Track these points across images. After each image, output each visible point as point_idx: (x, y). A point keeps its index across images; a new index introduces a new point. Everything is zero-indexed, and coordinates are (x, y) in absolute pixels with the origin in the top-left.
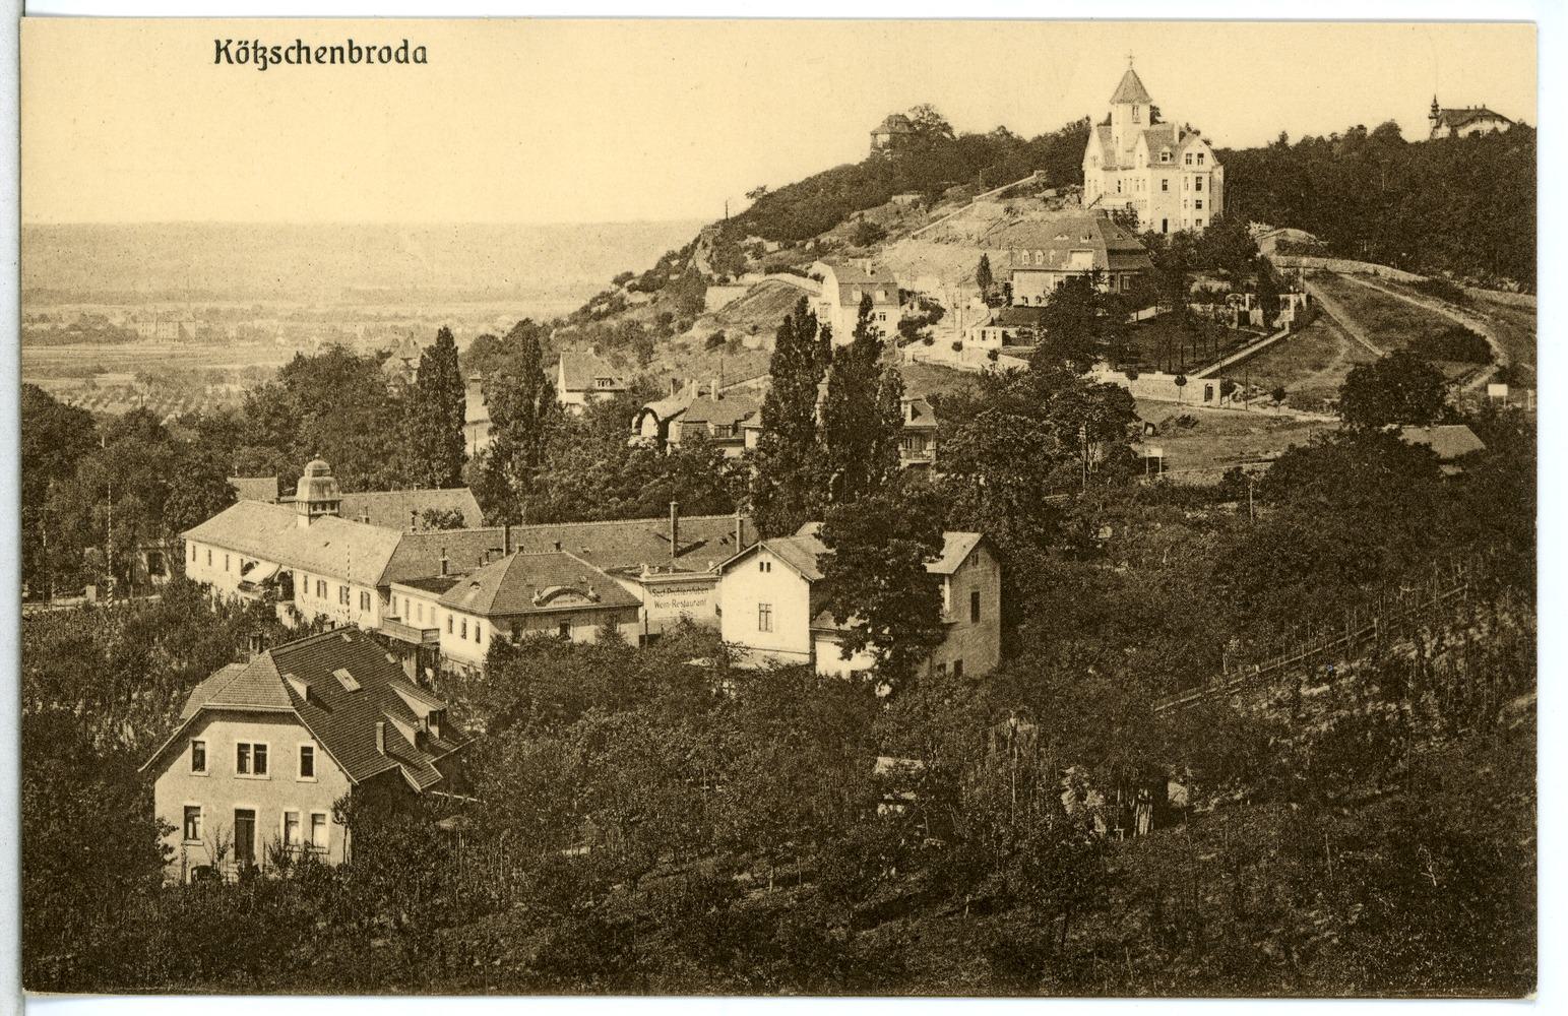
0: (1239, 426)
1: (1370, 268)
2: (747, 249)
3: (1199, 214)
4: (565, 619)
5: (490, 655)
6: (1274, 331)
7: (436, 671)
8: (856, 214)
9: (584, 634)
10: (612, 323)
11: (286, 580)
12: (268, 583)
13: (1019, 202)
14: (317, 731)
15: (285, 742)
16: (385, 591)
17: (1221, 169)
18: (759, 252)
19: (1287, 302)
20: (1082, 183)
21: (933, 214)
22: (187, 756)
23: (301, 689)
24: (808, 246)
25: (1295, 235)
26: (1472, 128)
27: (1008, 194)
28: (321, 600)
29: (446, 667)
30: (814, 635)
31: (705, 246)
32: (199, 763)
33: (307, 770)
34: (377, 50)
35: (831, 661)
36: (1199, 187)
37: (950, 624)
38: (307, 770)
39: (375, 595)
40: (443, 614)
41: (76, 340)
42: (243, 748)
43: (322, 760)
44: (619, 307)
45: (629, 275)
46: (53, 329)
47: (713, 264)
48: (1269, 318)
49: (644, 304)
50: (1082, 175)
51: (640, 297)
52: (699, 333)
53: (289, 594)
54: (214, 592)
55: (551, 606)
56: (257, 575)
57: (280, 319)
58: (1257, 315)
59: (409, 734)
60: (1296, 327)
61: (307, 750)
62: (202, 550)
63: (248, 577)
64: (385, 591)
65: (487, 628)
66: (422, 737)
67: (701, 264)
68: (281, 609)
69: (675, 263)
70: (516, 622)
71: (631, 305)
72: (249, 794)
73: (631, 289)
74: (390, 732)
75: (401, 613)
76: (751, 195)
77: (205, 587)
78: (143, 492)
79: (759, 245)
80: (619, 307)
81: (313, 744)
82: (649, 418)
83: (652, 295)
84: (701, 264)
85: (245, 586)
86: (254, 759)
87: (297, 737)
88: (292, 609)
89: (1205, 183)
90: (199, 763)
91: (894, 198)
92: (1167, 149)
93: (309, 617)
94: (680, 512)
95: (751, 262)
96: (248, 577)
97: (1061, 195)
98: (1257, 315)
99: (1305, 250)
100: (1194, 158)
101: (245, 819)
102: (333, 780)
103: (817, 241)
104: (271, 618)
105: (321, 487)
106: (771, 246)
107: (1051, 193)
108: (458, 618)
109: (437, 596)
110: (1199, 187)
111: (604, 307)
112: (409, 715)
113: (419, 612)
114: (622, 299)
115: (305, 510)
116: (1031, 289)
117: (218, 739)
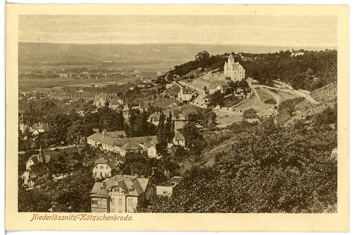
0: (234, 116)
2: (174, 77)
4: (134, 150)
5: (126, 154)
6: (246, 99)
7: (120, 156)
8: (192, 71)
10: (151, 89)
11: (101, 144)
12: (99, 145)
13: (214, 74)
14: (108, 165)
15: (105, 166)
16: (113, 146)
17: (245, 70)
18: (176, 77)
19: (248, 94)
20: (224, 71)
21: (202, 74)
22: (96, 167)
23: (106, 161)
24: (184, 76)
25: (255, 81)
26: (297, 54)
28: (105, 147)
29: (120, 156)
30: (156, 154)
31: (167, 76)
32: (97, 168)
33: (107, 168)
34: (120, 218)
36: (240, 73)
37: (170, 153)
38: (107, 168)
39: (112, 147)
41: (46, 77)
42: (101, 167)
43: (109, 167)
44: (152, 86)
46: (41, 75)
47: (168, 79)
48: (246, 97)
49: (156, 86)
50: (224, 70)
51: (156, 84)
52: (164, 94)
53: (101, 146)
54: (91, 145)
55: (133, 149)
56: (97, 144)
57: (89, 71)
58: (244, 96)
59: (117, 165)
60: (249, 98)
61: (107, 167)
62: (90, 140)
63: (96, 144)
64: (113, 146)
65: (125, 151)
66: (118, 165)
67: (166, 79)
68: (100, 148)
69: (162, 78)
70: (129, 150)
71: (154, 86)
72: (102, 170)
73: (154, 83)
74: (115, 165)
75: (115, 149)
76: (174, 67)
77: (91, 145)
78: (81, 132)
79: (176, 76)
80: (152, 86)
81: (107, 166)
82: (150, 117)
83: (158, 84)
84: (166, 79)
85: (96, 145)
86: (102, 167)
87: (106, 165)
88: (102, 148)
90: (97, 168)
91: (198, 68)
92: (236, 67)
93: (104, 149)
94: (149, 136)
95: (174, 79)
96: (96, 144)
97: (221, 73)
98: (244, 96)
99: (256, 84)
100: (240, 69)
101: (101, 173)
102: (110, 170)
103: (185, 76)
104: (99, 149)
105: (105, 133)
106: (178, 76)
107: (219, 73)
108: (122, 150)
109: (120, 147)
110: (240, 73)
111: (150, 86)
112: (117, 163)
113: (117, 149)
114: (153, 84)
115: (103, 135)
116: (212, 92)
117: (99, 166)
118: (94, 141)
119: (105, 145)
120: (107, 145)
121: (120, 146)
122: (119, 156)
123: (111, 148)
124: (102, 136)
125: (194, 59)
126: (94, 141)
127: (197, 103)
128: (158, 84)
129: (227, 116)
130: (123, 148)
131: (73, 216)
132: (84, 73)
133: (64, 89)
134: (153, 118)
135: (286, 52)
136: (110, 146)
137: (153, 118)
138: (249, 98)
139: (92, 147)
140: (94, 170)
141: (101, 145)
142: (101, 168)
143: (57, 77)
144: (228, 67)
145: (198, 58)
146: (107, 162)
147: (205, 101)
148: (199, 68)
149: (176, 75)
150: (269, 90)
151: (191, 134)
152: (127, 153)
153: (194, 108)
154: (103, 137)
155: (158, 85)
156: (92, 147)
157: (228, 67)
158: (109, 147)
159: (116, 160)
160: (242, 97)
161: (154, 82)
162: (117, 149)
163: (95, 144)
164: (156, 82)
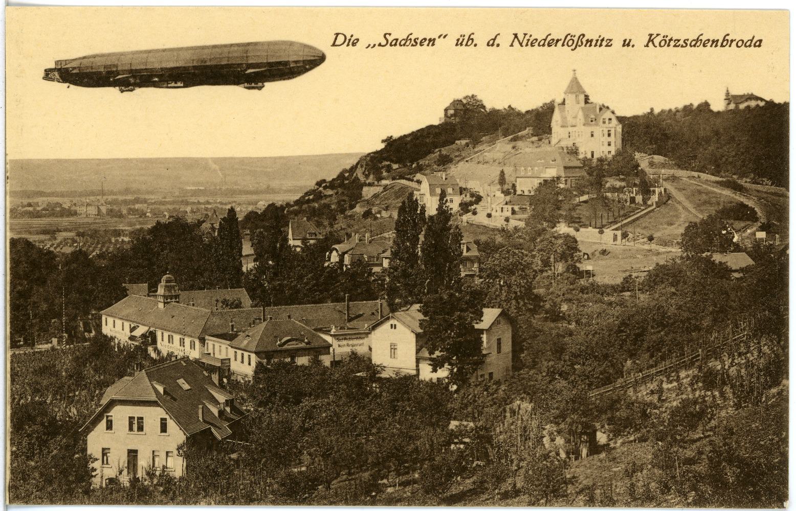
1: (696, 174)
2: (383, 167)
3: (610, 149)
5: (256, 372)
9: (303, 361)
11: (153, 335)
13: (520, 144)
14: (168, 410)
15: (153, 416)
17: (621, 126)
18: (389, 169)
20: (551, 133)
21: (476, 150)
22: (103, 423)
23: (161, 389)
25: (658, 159)
27: (515, 139)
28: (171, 345)
32: (109, 426)
35: (427, 373)
40: (231, 351)
43: (171, 424)
45: (324, 181)
48: (645, 201)
49: (331, 196)
50: (550, 129)
53: (154, 341)
56: (138, 332)
58: (639, 199)
59: (215, 411)
60: (658, 205)
62: (110, 320)
63: (134, 333)
64: (203, 341)
66: (221, 413)
69: (347, 175)
73: (325, 188)
74: (206, 411)
75: (211, 351)
82: (334, 253)
83: (336, 191)
85: (132, 338)
86: (136, 424)
89: (612, 133)
90: (109, 426)
91: (457, 142)
94: (350, 300)
95: (385, 174)
96: (134, 333)
97: (540, 140)
98: (639, 199)
100: (607, 121)
101: (133, 454)
102: (177, 435)
103: (418, 164)
104: (146, 356)
106: (395, 166)
107: (535, 139)
108: (239, 352)
109: (228, 342)
110: (609, 135)
112: (215, 402)
113: (220, 350)
116: (526, 186)
117: (120, 414)
118: (127, 325)
119: (166, 334)
120: (177, 338)
121: (229, 337)
122: (228, 378)
123: (192, 346)
124: (156, 303)
125: (436, 122)
126: (127, 325)
127: (489, 216)
128: (336, 191)
129: (604, 252)
130: (245, 342)
131: (605, 39)
132: (137, 206)
133: (79, 235)
134: (346, 253)
135: (700, 106)
136: (187, 341)
137: (346, 253)
138: (657, 203)
139: (119, 347)
140: (96, 441)
141: (151, 338)
142: (131, 429)
143: (72, 215)
144: (564, 118)
145: (452, 115)
146: (165, 391)
147: (513, 210)
148: (459, 139)
149: (388, 163)
150: (715, 185)
151: (516, 298)
152: (259, 365)
153: (479, 230)
154: (161, 305)
155: (337, 193)
156: (119, 347)
157: (564, 118)
158: (182, 343)
159: (214, 384)
160: (633, 200)
161: (323, 185)
162: (220, 350)
163: (129, 334)
164: (330, 185)
